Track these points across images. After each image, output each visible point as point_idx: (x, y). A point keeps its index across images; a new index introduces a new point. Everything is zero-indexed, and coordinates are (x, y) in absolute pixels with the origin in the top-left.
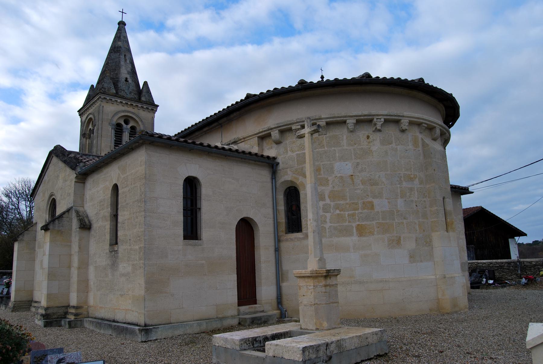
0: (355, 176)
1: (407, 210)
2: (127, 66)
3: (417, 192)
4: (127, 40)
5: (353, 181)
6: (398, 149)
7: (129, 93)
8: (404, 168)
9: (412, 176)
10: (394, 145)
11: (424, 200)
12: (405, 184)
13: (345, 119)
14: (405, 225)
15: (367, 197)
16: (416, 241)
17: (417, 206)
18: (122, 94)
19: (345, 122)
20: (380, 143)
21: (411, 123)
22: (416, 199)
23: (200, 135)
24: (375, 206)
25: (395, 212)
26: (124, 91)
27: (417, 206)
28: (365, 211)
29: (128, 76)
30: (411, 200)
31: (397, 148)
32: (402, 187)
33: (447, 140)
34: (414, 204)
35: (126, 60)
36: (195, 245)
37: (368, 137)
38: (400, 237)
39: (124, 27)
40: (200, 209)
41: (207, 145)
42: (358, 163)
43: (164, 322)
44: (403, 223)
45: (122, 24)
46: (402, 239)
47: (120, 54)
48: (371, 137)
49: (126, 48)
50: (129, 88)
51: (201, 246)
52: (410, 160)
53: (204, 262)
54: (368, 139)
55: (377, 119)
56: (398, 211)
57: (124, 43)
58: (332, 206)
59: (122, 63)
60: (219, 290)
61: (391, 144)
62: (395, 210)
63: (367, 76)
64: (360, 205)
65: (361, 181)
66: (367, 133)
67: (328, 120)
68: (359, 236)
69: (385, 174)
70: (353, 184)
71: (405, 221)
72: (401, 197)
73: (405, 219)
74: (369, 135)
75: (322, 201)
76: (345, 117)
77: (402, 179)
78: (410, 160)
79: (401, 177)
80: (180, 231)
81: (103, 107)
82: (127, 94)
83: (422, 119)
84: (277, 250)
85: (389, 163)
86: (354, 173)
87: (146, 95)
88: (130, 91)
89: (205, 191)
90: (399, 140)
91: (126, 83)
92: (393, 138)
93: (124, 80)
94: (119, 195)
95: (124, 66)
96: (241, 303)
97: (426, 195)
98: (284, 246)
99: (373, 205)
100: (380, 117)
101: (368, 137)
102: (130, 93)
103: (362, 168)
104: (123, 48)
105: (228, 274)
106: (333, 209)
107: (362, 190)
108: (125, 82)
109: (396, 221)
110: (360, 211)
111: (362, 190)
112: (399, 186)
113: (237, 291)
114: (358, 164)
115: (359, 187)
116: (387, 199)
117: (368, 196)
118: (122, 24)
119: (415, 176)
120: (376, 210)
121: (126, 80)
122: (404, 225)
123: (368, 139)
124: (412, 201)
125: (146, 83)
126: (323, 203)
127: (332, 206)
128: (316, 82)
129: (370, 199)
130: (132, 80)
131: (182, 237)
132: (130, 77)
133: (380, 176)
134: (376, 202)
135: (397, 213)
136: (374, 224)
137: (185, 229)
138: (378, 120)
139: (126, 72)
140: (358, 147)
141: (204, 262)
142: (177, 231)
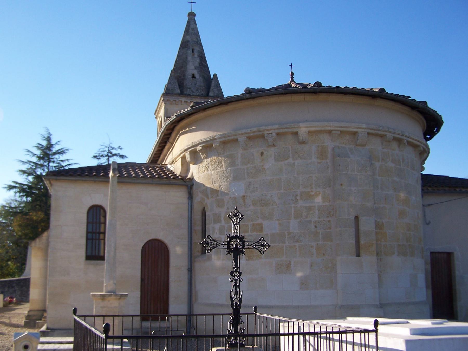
0: (247, 196)
1: (302, 232)
2: (195, 61)
3: (319, 210)
5: (245, 202)
6: (296, 164)
7: (196, 90)
8: (301, 184)
9: (312, 193)
10: (290, 160)
11: (329, 219)
12: (301, 203)
13: (235, 137)
14: (298, 249)
15: (257, 218)
16: (311, 266)
17: (316, 227)
18: (188, 92)
19: (236, 141)
20: (275, 159)
22: (316, 219)
24: (264, 228)
25: (286, 234)
26: (190, 88)
27: (316, 227)
28: (255, 233)
29: (195, 72)
30: (308, 220)
31: (294, 163)
32: (297, 207)
34: (313, 226)
35: (193, 55)
37: (262, 154)
38: (290, 262)
39: (193, 19)
42: (250, 182)
44: (295, 246)
45: (192, 15)
46: (292, 263)
47: (187, 49)
48: (265, 153)
49: (194, 41)
50: (195, 85)
52: (311, 175)
54: (261, 156)
55: (268, 134)
56: (289, 233)
57: (193, 35)
58: (226, 228)
59: (190, 58)
61: (286, 159)
62: (286, 232)
64: (250, 228)
65: (252, 202)
66: (261, 150)
68: (247, 260)
69: (278, 193)
70: (245, 205)
71: (297, 244)
72: (295, 218)
73: (298, 241)
74: (263, 151)
75: (219, 223)
76: (235, 135)
77: (298, 198)
78: (311, 175)
79: (297, 195)
81: (167, 109)
82: (193, 92)
84: (190, 270)
85: (283, 181)
86: (246, 193)
87: (215, 89)
88: (197, 88)
90: (297, 154)
91: (193, 80)
92: (290, 152)
93: (190, 77)
95: (191, 61)
96: (144, 317)
97: (333, 214)
98: (198, 265)
99: (262, 228)
100: (271, 132)
101: (262, 154)
102: (197, 90)
103: (254, 187)
104: (191, 42)
106: (226, 232)
107: (252, 212)
108: (192, 78)
109: (287, 244)
110: (250, 233)
111: (252, 212)
112: (293, 205)
114: (250, 183)
115: (249, 208)
116: (278, 220)
117: (258, 217)
118: (192, 15)
119: (318, 193)
120: (265, 233)
121: (193, 76)
122: (296, 248)
123: (261, 156)
124: (310, 222)
125: (215, 75)
126: (220, 224)
127: (226, 228)
129: (260, 221)
130: (200, 75)
131: (84, 258)
132: (198, 72)
133: (271, 196)
134: (265, 223)
135: (288, 235)
136: (287, 243)
138: (269, 135)
139: (193, 67)
140: (252, 166)
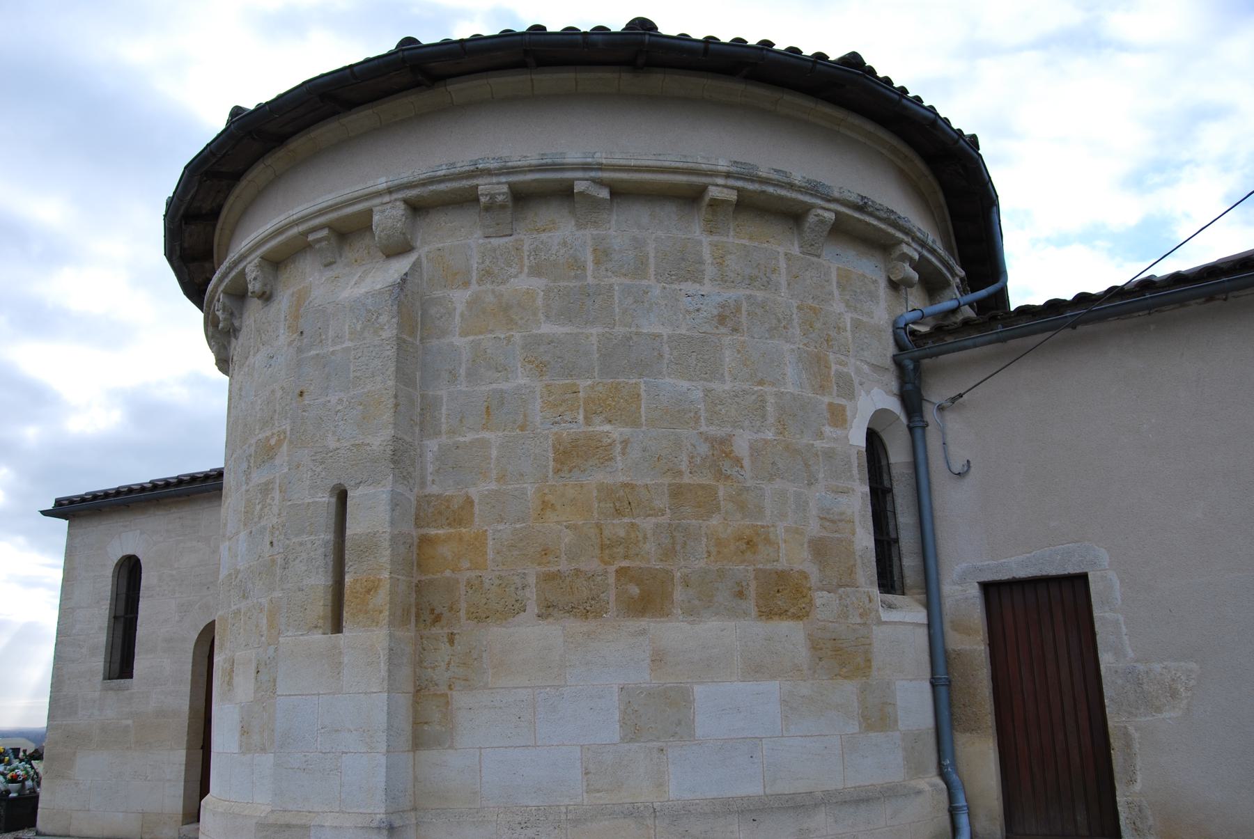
4: (211, 329)
21: (417, 208)
23: (975, 322)
33: (509, 185)
36: (118, 690)
40: (115, 618)
41: (152, 486)
43: (60, 833)
51: (129, 691)
53: (130, 722)
60: (149, 781)
63: (642, 26)
67: (750, 186)
80: (98, 663)
83: (291, 227)
89: (148, 579)
94: (1044, 573)
105: (169, 748)
113: (182, 788)
128: (810, 54)
137: (109, 661)
141: (130, 722)
142: (95, 664)
